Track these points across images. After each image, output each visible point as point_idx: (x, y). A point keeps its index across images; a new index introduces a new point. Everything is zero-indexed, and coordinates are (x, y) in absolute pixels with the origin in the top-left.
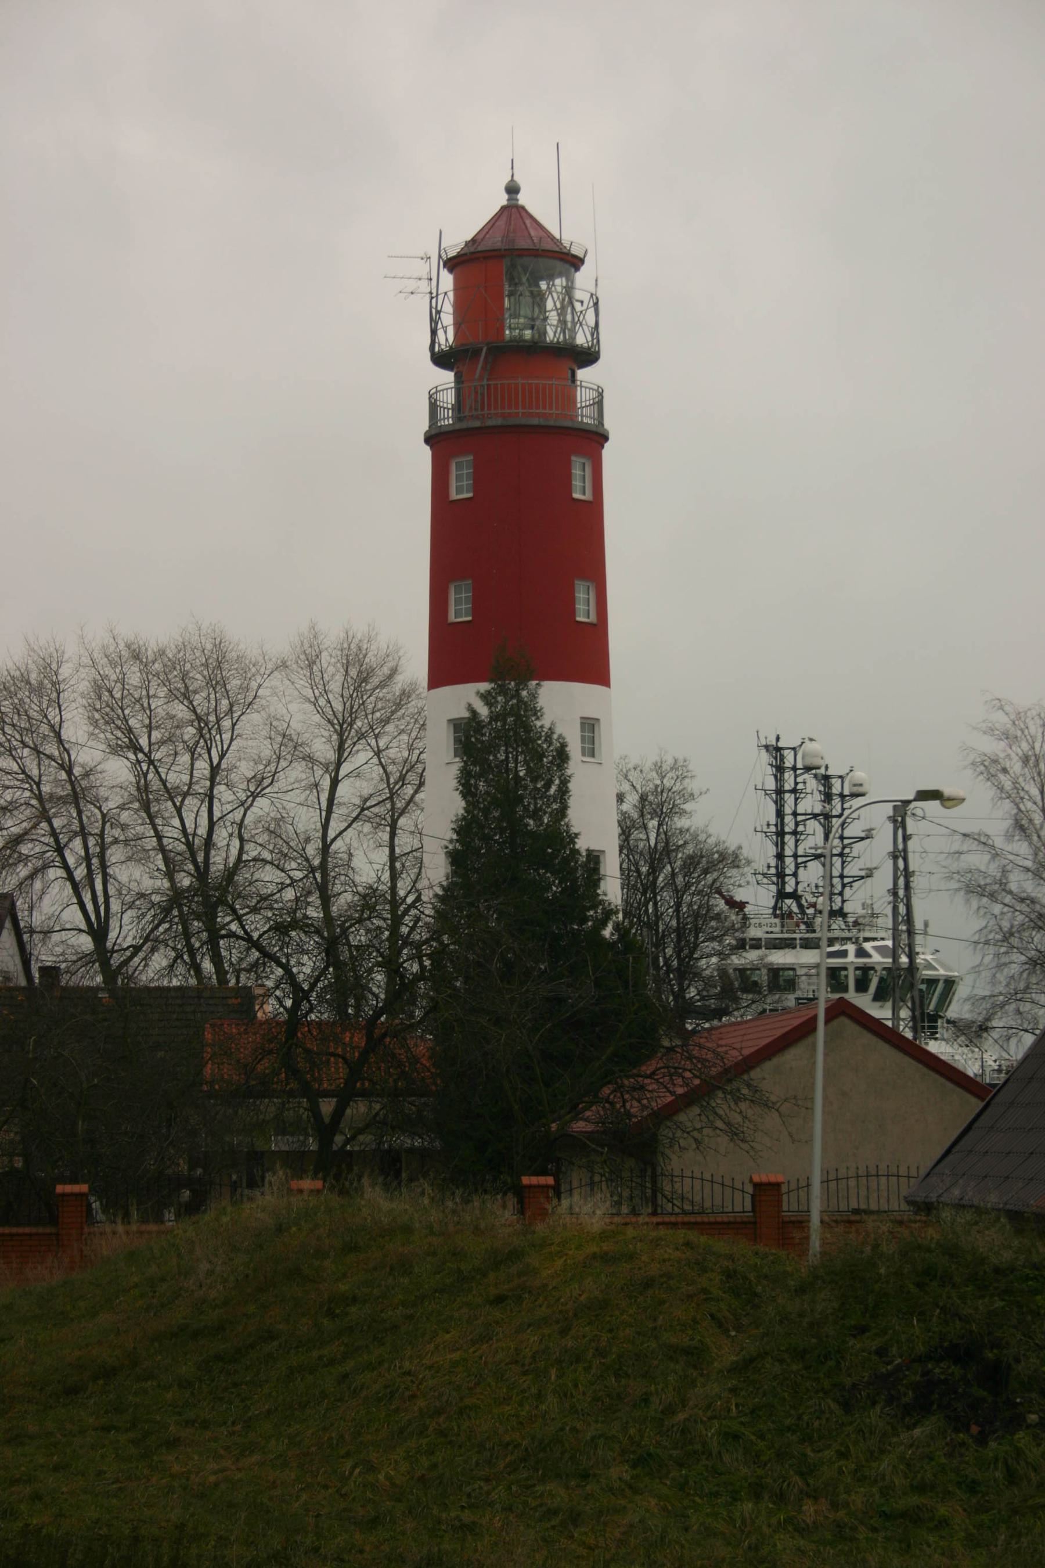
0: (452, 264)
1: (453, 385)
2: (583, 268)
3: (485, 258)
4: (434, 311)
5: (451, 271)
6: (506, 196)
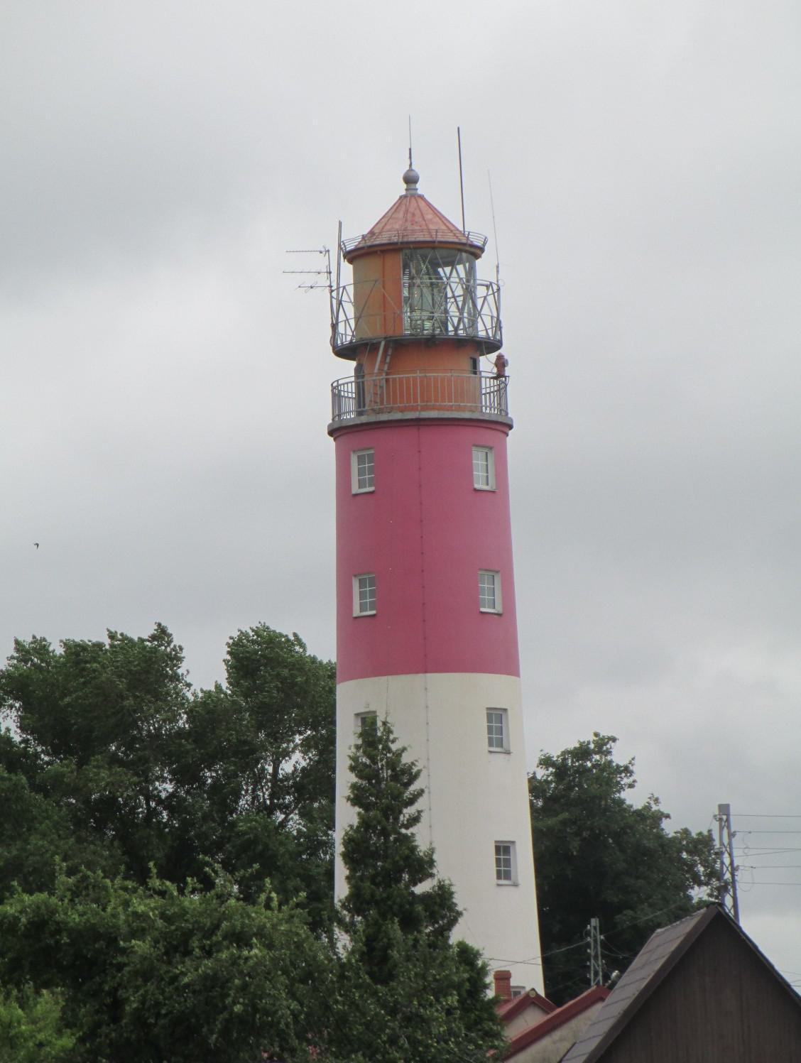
0: (353, 256)
1: (353, 379)
2: (483, 255)
3: (382, 252)
4: (334, 302)
5: (350, 261)
6: (405, 186)
